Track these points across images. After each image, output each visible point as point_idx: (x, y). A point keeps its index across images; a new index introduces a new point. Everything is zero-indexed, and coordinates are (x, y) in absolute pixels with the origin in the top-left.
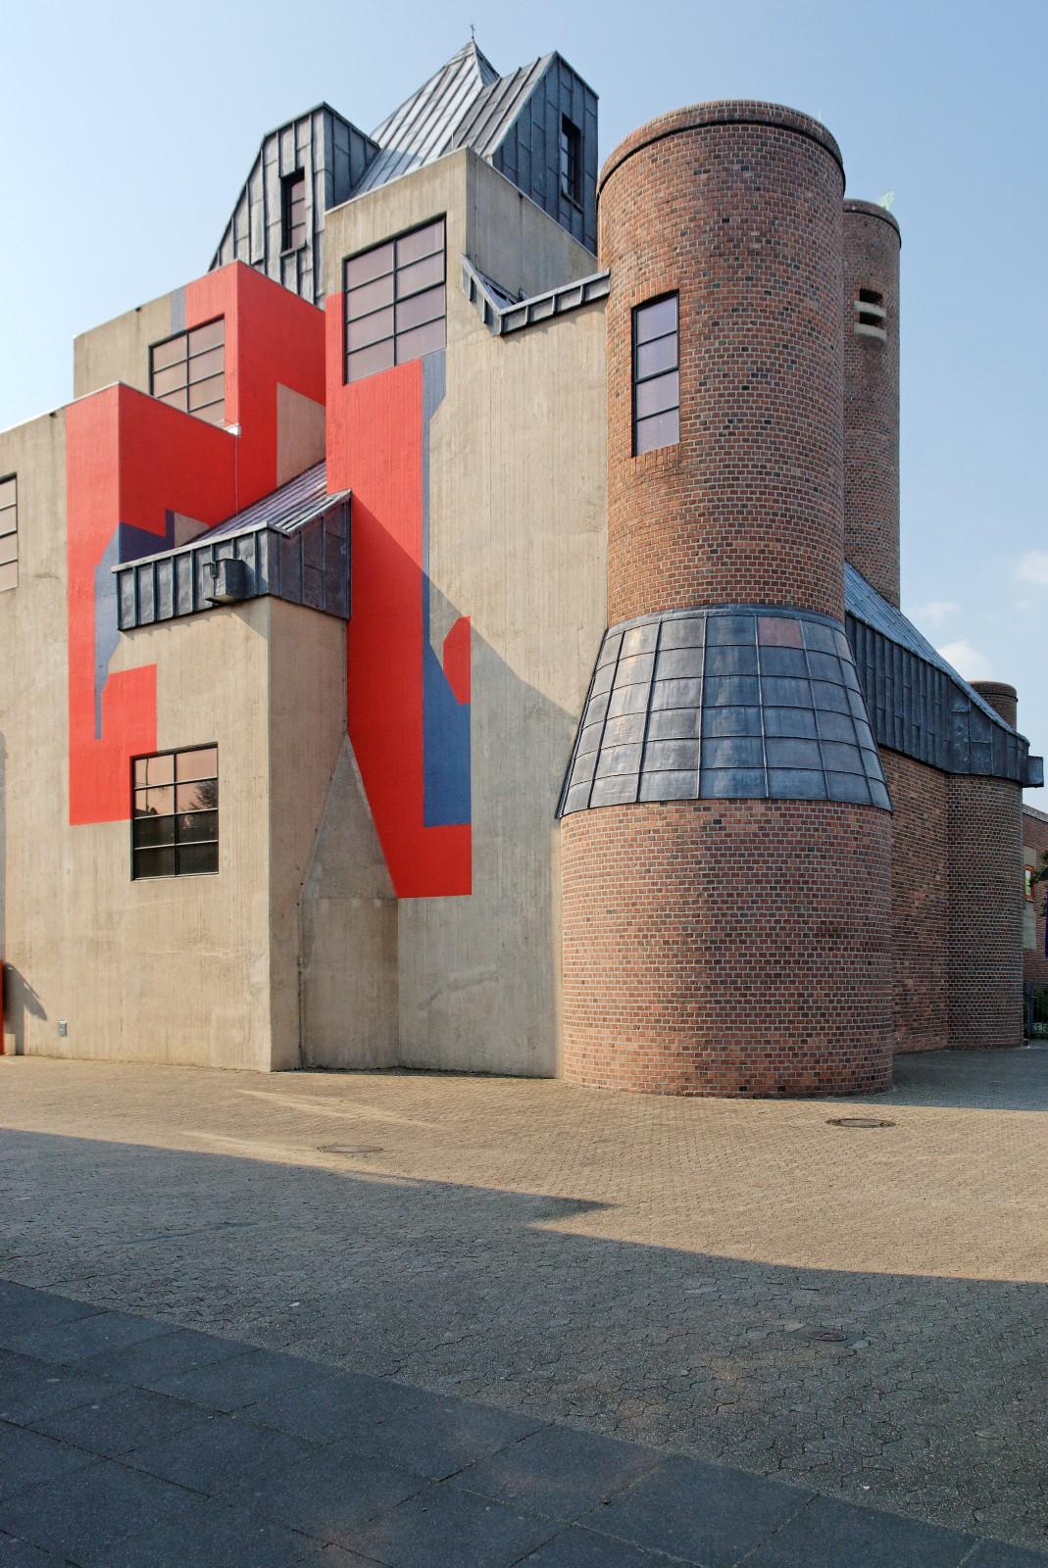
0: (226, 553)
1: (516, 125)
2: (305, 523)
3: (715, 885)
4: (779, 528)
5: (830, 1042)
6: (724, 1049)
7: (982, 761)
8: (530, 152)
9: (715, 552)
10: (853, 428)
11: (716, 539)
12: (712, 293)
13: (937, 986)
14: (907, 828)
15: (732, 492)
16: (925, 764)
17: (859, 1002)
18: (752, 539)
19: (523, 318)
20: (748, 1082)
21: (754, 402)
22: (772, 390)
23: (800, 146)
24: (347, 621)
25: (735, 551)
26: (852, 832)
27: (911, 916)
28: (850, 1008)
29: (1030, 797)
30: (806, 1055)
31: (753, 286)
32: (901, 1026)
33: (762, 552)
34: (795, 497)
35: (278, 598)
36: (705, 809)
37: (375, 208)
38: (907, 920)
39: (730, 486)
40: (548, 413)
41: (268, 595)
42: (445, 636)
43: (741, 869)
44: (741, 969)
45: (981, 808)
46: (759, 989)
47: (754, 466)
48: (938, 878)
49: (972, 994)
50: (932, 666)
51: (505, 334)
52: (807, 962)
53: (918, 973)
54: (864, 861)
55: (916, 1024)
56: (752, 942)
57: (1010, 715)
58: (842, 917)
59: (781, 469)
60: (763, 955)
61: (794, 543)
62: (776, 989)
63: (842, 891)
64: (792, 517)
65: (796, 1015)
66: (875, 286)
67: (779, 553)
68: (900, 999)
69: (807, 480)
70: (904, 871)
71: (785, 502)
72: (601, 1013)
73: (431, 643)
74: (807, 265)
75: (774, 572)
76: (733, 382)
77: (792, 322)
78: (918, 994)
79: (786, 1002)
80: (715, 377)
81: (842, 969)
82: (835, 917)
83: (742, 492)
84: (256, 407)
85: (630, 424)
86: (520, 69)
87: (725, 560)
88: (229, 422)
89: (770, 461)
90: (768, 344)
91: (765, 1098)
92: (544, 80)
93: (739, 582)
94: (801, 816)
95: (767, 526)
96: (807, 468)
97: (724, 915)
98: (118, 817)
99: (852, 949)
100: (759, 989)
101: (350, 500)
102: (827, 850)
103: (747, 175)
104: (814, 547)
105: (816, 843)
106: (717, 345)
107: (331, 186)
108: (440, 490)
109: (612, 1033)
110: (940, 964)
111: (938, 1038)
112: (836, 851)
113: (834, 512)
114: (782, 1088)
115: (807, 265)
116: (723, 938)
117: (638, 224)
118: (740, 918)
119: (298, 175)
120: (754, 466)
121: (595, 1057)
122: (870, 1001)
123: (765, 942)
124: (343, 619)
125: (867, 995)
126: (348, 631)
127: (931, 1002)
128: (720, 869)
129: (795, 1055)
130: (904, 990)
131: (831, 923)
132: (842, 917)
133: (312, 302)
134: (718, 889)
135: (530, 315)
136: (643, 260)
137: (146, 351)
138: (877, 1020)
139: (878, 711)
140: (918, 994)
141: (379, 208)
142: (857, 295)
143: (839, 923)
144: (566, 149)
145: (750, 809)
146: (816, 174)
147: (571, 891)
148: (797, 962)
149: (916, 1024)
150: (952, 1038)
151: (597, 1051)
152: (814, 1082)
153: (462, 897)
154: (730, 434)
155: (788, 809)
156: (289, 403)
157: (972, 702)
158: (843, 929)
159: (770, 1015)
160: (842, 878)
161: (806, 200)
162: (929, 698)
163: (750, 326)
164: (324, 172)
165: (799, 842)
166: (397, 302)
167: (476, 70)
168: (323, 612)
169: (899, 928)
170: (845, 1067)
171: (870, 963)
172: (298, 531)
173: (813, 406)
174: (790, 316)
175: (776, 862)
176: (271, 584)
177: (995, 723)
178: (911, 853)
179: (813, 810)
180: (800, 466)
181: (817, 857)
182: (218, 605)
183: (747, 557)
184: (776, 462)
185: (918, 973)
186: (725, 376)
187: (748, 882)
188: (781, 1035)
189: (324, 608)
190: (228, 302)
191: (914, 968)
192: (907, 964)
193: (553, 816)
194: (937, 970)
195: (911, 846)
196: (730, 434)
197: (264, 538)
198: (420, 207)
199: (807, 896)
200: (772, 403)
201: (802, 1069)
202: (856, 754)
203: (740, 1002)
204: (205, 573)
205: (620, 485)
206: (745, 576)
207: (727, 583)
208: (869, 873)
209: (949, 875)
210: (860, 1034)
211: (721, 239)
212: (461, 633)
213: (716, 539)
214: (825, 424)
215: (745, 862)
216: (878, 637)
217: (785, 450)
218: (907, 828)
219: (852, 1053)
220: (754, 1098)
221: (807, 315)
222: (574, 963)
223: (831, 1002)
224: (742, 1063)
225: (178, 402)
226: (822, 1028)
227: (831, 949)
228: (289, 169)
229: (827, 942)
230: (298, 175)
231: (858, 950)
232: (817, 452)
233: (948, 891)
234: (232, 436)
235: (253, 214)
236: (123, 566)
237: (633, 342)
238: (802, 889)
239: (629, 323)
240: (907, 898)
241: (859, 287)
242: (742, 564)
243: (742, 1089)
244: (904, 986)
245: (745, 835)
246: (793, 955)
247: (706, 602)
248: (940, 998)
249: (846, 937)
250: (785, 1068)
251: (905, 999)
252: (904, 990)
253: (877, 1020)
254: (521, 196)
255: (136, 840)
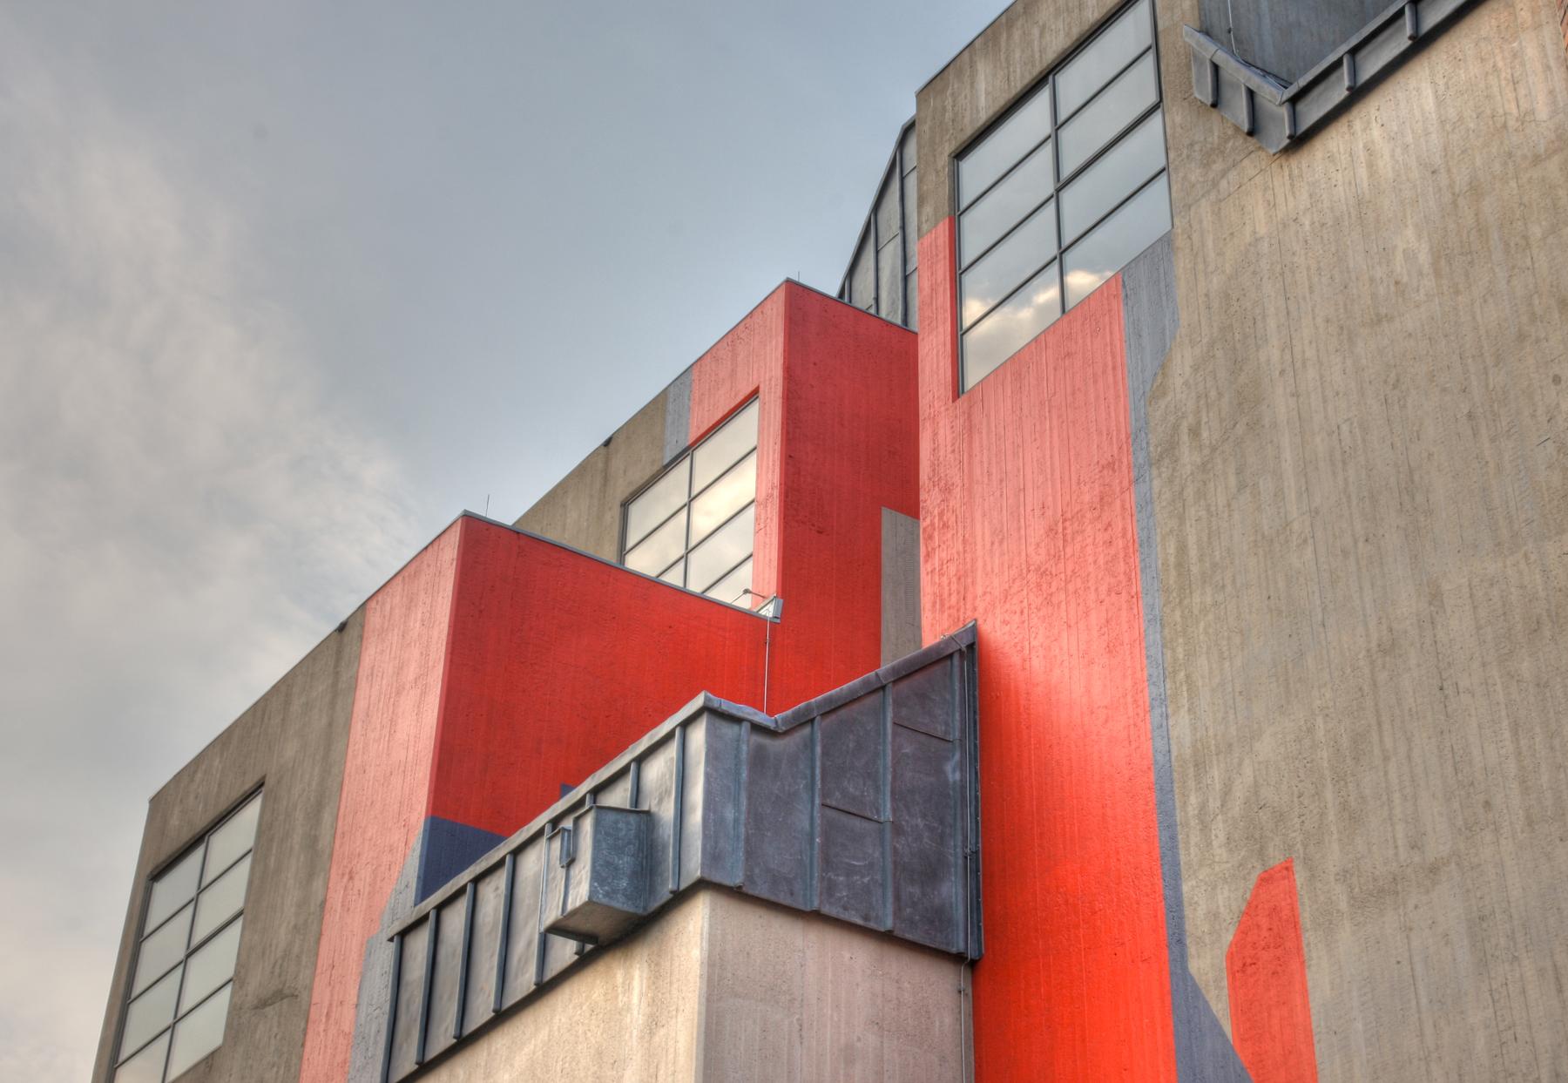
19: (1341, 79)
35: (736, 893)
37: (1009, 37)
40: (1435, 264)
41: (702, 885)
101: (971, 647)
124: (958, 959)
126: (976, 998)
135: (1354, 73)
141: (1017, 34)
166: (1062, 186)
168: (888, 938)
189: (889, 923)
235: (882, 264)
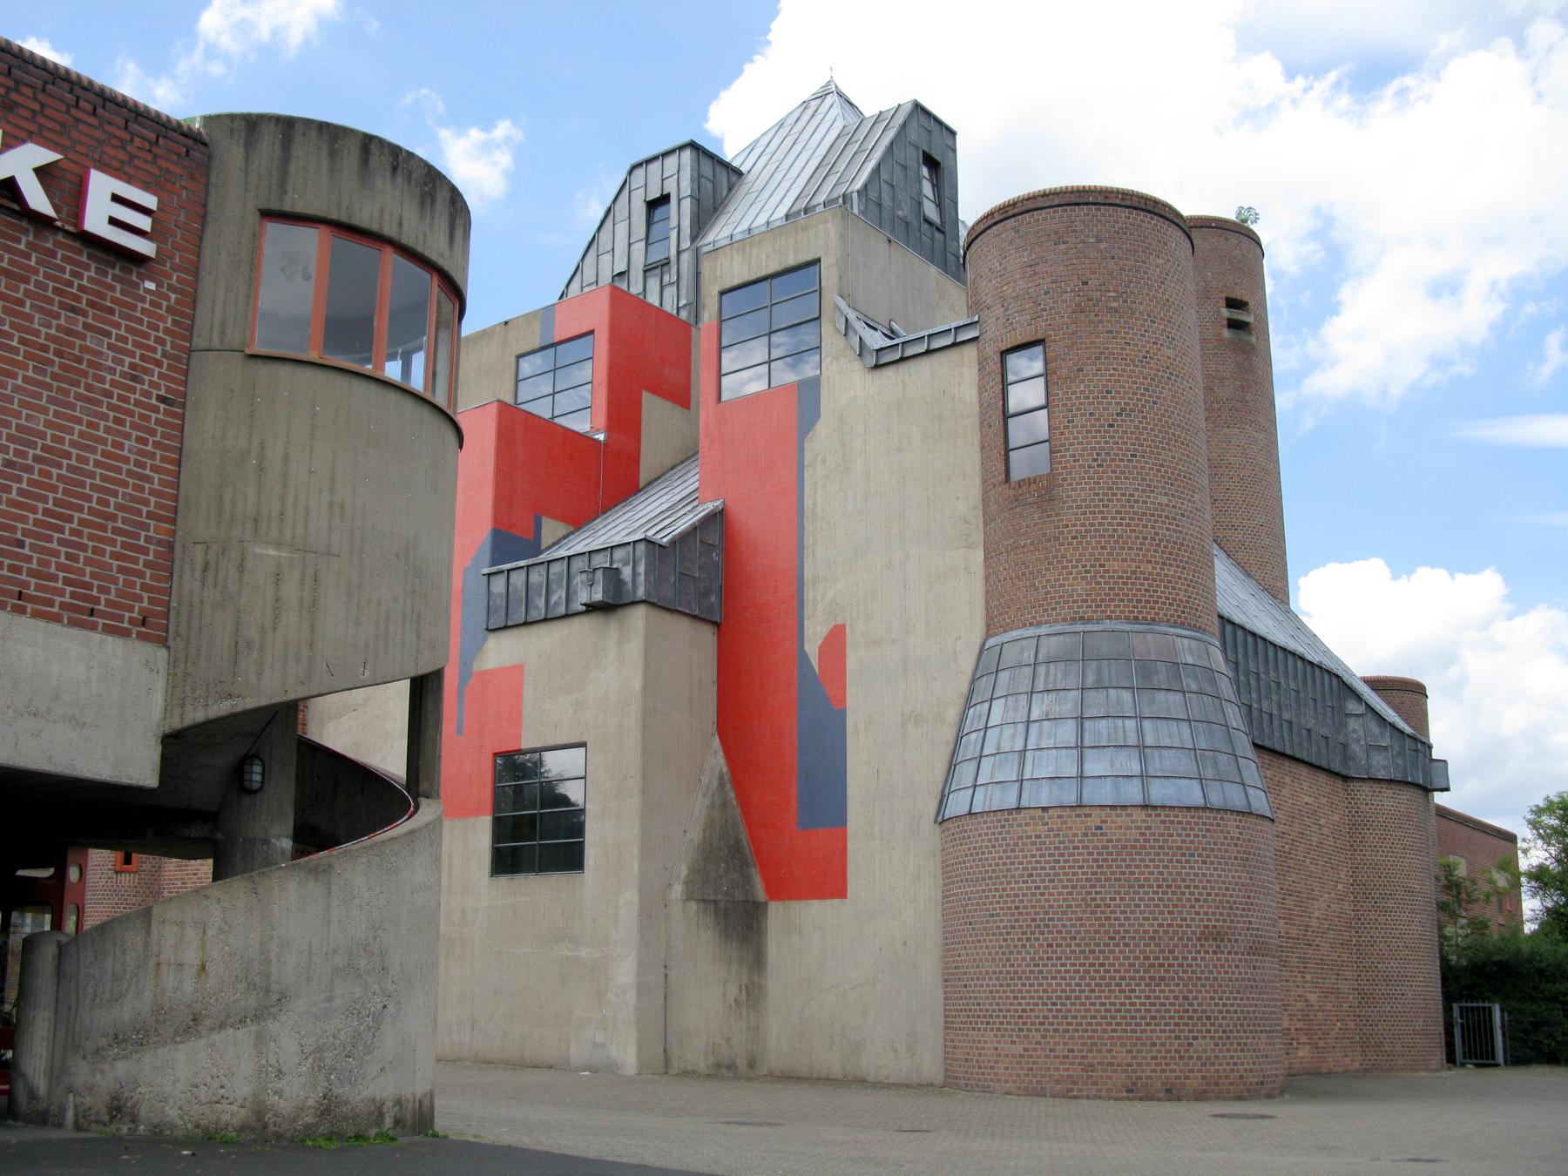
0: (600, 561)
1: (878, 166)
2: (680, 533)
3: (1098, 889)
4: (1149, 550)
5: (1216, 1045)
6: (1110, 1051)
7: (1381, 765)
8: (892, 186)
9: (1089, 572)
10: (1228, 427)
11: (1089, 560)
12: (1076, 343)
13: (1344, 1002)
14: (1302, 834)
15: (1103, 518)
16: (1319, 768)
17: (1245, 1006)
18: (1123, 560)
20: (1134, 1084)
21: (1119, 438)
22: (1136, 428)
23: (1149, 223)
24: (717, 625)
25: (1108, 571)
26: (1232, 838)
27: (1311, 926)
28: (1236, 1012)
29: (1440, 798)
30: (1191, 1058)
31: (1113, 338)
32: (1304, 1043)
33: (1135, 572)
34: (1164, 523)
36: (1086, 815)
38: (1306, 931)
39: (1100, 512)
41: (644, 602)
42: (820, 642)
43: (1124, 873)
44: (1125, 971)
45: (1383, 814)
46: (1144, 991)
47: (1122, 495)
48: (1340, 887)
49: (1384, 1012)
50: (1321, 668)
51: (877, 367)
52: (1191, 965)
53: (1321, 988)
54: (1245, 866)
55: (1321, 1043)
56: (1136, 945)
57: (1419, 717)
58: (1225, 921)
59: (1149, 497)
60: (1148, 958)
61: (1164, 564)
62: (1160, 991)
63: (1225, 895)
64: (1161, 540)
65: (1181, 1018)
66: (1238, 294)
67: (1150, 574)
68: (1303, 1015)
69: (1174, 507)
70: (1302, 879)
71: (1153, 527)
72: (985, 1016)
73: (806, 648)
74: (1162, 319)
75: (1146, 590)
76: (1098, 420)
77: (1151, 369)
78: (1324, 1011)
79: (1171, 1004)
80: (1082, 415)
81: (1227, 973)
82: (1217, 921)
83: (1113, 518)
84: (623, 416)
85: (1003, 453)
86: (881, 112)
87: (1099, 579)
88: (598, 431)
89: (1137, 490)
90: (1130, 388)
91: (1151, 1100)
92: (904, 126)
93: (1113, 600)
94: (1180, 822)
95: (1137, 549)
96: (1173, 496)
97: (1107, 919)
98: (477, 812)
99: (1236, 953)
100: (1144, 991)
102: (1208, 856)
103: (1103, 246)
104: (1184, 568)
105: (1196, 849)
106: (1082, 388)
107: (696, 209)
108: (815, 504)
109: (996, 1036)
110: (1346, 980)
111: (1348, 1059)
112: (1216, 857)
113: (1202, 534)
114: (1168, 1091)
115: (1162, 319)
116: (1107, 941)
117: (1004, 282)
118: (1122, 921)
119: (664, 199)
120: (1122, 495)
121: (977, 1061)
122: (1256, 1006)
123: (1149, 945)
125: (1253, 999)
127: (1338, 1020)
128: (1102, 873)
129: (1182, 1058)
130: (1307, 1006)
131: (1215, 927)
132: (1225, 921)
133: (675, 312)
134: (1100, 893)
136: (1010, 312)
137: (514, 359)
138: (1264, 1025)
139: (1264, 715)
140: (1324, 1011)
141: (754, 251)
142: (1223, 303)
143: (1222, 927)
144: (932, 197)
145: (1131, 815)
146: (1165, 244)
147: (950, 896)
148: (1181, 965)
149: (1321, 1043)
150: (1364, 1060)
151: (980, 1055)
152: (1201, 1084)
153: (836, 901)
154: (1099, 466)
155: (1168, 816)
156: (654, 409)
157: (1366, 703)
158: (1226, 934)
159: (1155, 1018)
160: (1224, 882)
161: (1157, 266)
162: (1319, 701)
163: (1112, 372)
164: (689, 199)
165: (1179, 848)
167: (836, 110)
168: (695, 617)
169: (1298, 939)
170: (1232, 1071)
171: (1254, 968)
172: (673, 542)
173: (1176, 441)
174: (1149, 363)
175: (1158, 867)
176: (647, 592)
177: (1392, 726)
178: (1308, 861)
179: (1193, 817)
180: (1166, 494)
181: (1197, 862)
182: (592, 608)
183: (1119, 577)
184: (1144, 491)
185: (1321, 988)
186: (1091, 414)
187: (1130, 887)
188: (1167, 1038)
189: (697, 612)
190: (597, 316)
191: (1317, 983)
192: (1308, 977)
193: (932, 821)
194: (1344, 986)
195: (1309, 853)
196: (1099, 466)
197: (641, 547)
198: (795, 252)
199: (1189, 900)
200: (1137, 439)
201: (1189, 1071)
202: (1233, 763)
203: (1125, 1004)
204: (579, 579)
205: (995, 507)
206: (1119, 595)
207: (1102, 600)
208: (1251, 879)
209: (1352, 885)
210: (1247, 1038)
211: (1082, 299)
212: (836, 640)
213: (1089, 560)
214: (1188, 456)
215: (1127, 867)
216: (1259, 641)
217: (1151, 480)
218: (1302, 834)
219: (1239, 1058)
220: (1141, 1099)
221: (1165, 362)
222: (956, 968)
223: (1217, 1005)
224: (1129, 1065)
225: (542, 410)
226: (1208, 1031)
227: (1214, 952)
228: (654, 194)
229: (1211, 946)
230: (664, 199)
231: (1243, 954)
232: (1182, 481)
233: (1353, 902)
234: (598, 441)
236: (494, 569)
237: (1003, 380)
238: (1183, 893)
239: (999, 365)
240: (1306, 907)
241: (1224, 295)
242: (1115, 583)
243: (1129, 1091)
244: (1306, 1001)
245: (1126, 840)
246: (1177, 958)
247: (1082, 618)
248: (1348, 1016)
249: (1230, 941)
250: (1171, 1071)
251: (1308, 1015)
252: (1307, 1006)
253: (1264, 1025)
254: (890, 241)
255: (497, 836)
